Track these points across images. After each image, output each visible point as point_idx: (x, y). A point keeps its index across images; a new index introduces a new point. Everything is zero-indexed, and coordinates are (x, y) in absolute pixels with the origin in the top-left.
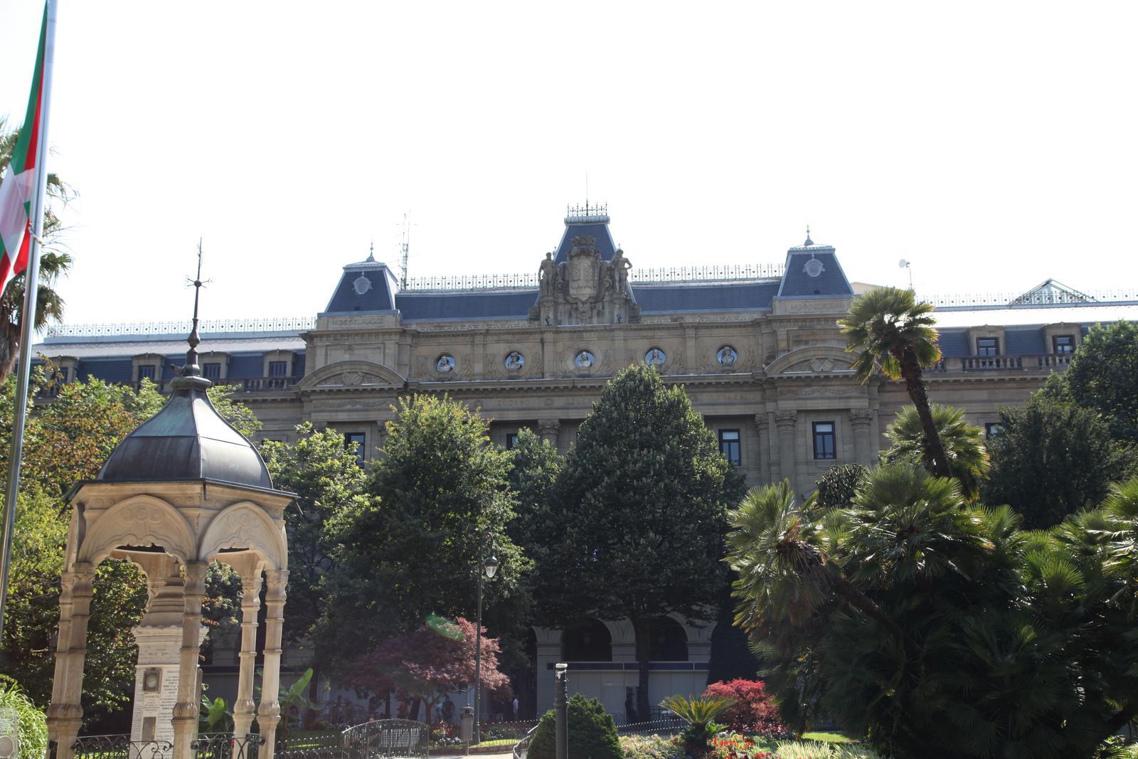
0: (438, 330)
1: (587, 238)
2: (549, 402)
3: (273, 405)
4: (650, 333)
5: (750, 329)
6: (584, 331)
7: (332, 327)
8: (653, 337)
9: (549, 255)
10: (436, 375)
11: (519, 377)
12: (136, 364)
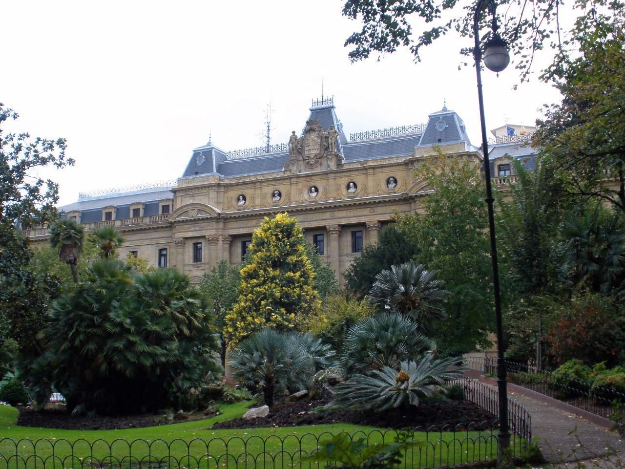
0: (237, 182)
1: (322, 118)
2: (332, 215)
3: (162, 230)
4: (348, 174)
5: (404, 167)
6: (312, 176)
7: (185, 185)
8: (350, 176)
9: (294, 132)
10: (237, 207)
11: (316, 201)
12: (104, 212)
